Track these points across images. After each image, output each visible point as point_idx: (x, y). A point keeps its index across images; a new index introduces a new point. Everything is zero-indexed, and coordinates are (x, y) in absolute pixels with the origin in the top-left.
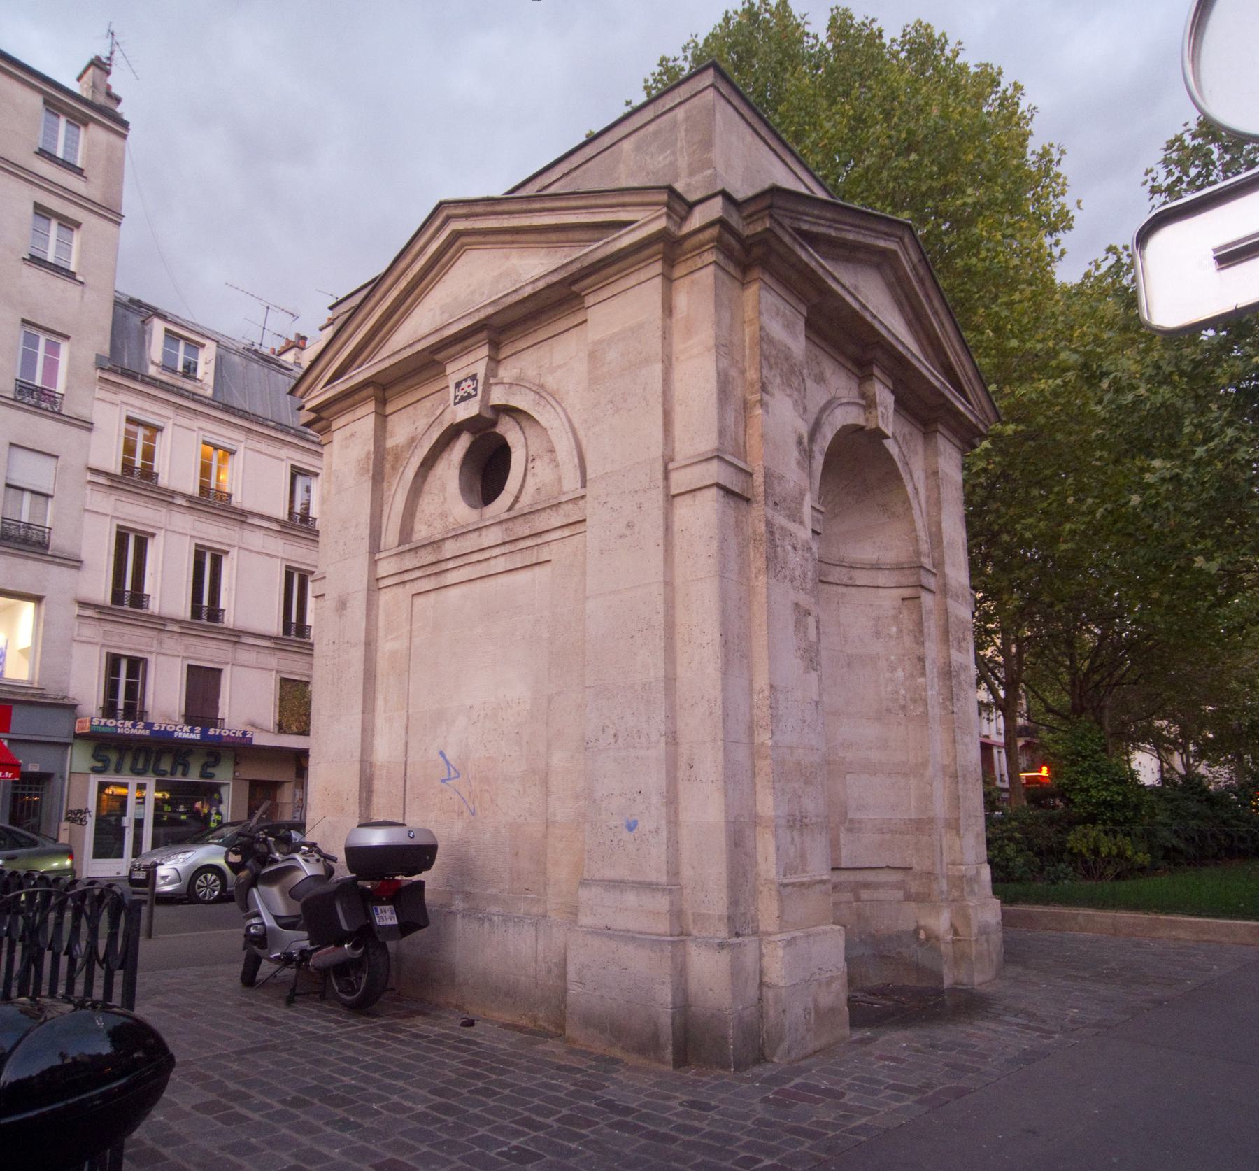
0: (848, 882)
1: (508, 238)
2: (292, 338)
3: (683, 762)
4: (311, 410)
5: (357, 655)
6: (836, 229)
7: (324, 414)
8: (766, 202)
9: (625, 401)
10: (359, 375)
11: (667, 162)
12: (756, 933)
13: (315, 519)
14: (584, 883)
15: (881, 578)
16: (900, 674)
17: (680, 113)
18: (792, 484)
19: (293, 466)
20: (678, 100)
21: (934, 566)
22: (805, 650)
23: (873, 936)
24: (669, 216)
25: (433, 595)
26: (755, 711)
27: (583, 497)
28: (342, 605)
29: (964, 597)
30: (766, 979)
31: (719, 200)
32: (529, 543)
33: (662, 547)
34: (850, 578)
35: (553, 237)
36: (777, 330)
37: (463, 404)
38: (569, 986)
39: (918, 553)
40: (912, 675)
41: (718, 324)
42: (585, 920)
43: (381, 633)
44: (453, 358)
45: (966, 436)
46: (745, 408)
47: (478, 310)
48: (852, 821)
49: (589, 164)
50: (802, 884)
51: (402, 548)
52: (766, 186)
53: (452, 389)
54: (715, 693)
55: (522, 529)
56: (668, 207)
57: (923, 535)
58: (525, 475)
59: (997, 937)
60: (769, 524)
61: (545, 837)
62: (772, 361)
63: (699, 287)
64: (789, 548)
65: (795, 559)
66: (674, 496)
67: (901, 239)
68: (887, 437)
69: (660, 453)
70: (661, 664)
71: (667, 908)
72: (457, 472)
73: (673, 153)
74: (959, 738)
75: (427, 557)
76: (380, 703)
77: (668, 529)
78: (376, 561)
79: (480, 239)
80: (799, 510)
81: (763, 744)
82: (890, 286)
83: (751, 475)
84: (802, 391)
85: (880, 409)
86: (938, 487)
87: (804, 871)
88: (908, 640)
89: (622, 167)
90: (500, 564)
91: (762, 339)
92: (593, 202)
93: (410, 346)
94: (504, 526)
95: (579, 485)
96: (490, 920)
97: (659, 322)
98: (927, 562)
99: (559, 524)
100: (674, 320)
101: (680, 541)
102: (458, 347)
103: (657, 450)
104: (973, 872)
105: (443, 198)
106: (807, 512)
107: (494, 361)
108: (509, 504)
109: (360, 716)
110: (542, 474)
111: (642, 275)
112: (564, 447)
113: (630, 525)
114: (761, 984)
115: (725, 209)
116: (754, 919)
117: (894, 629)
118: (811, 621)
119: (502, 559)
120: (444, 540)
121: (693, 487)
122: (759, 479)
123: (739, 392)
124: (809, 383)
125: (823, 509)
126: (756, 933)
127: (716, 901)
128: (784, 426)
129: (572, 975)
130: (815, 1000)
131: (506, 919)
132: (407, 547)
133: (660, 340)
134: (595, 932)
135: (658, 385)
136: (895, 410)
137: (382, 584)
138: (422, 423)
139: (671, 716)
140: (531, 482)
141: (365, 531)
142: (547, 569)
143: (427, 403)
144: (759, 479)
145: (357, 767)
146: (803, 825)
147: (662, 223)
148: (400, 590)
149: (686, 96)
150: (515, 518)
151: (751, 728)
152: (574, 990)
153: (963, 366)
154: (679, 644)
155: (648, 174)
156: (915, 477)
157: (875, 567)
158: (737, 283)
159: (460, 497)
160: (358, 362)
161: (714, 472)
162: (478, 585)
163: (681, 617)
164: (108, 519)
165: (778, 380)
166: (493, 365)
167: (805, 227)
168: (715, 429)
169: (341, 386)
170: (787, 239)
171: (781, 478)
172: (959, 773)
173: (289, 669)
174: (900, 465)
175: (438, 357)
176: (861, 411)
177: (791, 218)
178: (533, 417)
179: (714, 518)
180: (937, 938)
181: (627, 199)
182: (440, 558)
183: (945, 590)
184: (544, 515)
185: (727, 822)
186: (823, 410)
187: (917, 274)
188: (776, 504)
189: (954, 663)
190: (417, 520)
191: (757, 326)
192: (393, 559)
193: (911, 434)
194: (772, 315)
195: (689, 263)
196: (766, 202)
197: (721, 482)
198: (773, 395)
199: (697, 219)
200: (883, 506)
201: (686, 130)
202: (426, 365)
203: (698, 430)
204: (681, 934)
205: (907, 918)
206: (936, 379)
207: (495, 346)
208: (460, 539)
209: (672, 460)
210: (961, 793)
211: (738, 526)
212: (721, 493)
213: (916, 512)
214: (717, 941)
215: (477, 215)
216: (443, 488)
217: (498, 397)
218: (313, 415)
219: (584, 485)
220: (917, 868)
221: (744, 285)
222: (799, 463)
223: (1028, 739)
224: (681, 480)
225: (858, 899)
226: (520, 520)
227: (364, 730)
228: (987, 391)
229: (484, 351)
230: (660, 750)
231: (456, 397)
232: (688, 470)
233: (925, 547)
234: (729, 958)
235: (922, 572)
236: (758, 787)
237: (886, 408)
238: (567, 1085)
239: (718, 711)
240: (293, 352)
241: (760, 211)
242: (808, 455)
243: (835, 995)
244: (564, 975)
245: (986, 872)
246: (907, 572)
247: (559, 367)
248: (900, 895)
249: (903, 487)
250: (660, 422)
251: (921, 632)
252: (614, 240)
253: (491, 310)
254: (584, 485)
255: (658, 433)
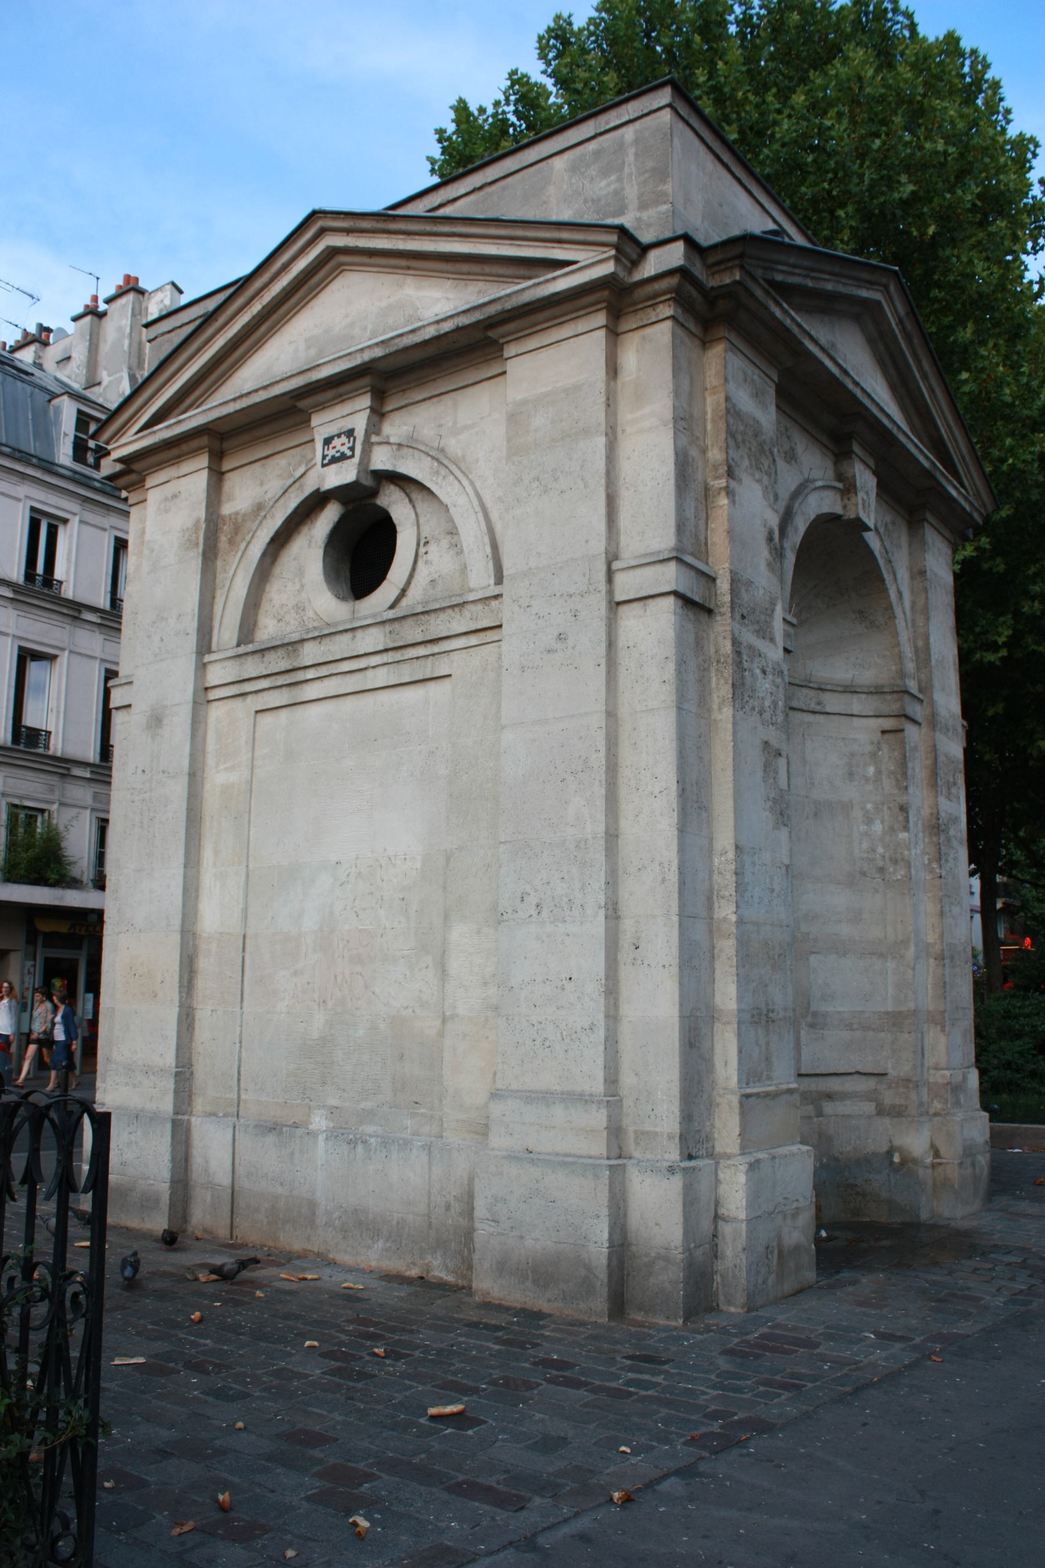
0: (815, 1091)
1: (403, 263)
2: (32, 329)
3: (626, 941)
4: (120, 460)
5: (178, 789)
6: (812, 278)
7: (136, 466)
8: (738, 250)
9: (556, 480)
10: (193, 419)
11: (613, 187)
12: (711, 1155)
13: (61, 583)
14: (495, 1095)
15: (857, 704)
16: (878, 827)
17: (629, 133)
18: (761, 592)
19: (33, 509)
20: (626, 118)
21: (920, 691)
22: (775, 801)
23: (837, 1159)
24: (617, 259)
25: (284, 714)
26: (715, 877)
27: (497, 597)
28: (156, 721)
29: (955, 730)
30: (722, 1211)
31: (679, 247)
32: (421, 651)
33: (603, 667)
34: (819, 704)
35: (465, 267)
36: (745, 401)
37: (334, 467)
38: (477, 1225)
39: (902, 674)
40: (892, 829)
41: (676, 393)
42: (498, 1140)
43: (210, 760)
44: (322, 407)
45: (958, 527)
46: (706, 496)
47: (362, 350)
48: (815, 1014)
49: (510, 179)
50: (767, 1095)
51: (242, 649)
52: (736, 232)
53: (319, 445)
54: (670, 855)
55: (412, 632)
56: (618, 249)
57: (908, 651)
58: (415, 562)
59: (983, 1160)
60: (735, 642)
61: (441, 1034)
62: (740, 438)
63: (652, 347)
64: (758, 671)
65: (764, 686)
66: (618, 604)
67: (886, 287)
68: (867, 529)
69: (603, 549)
70: (601, 816)
71: (605, 1124)
72: (320, 553)
73: (620, 180)
74: (946, 909)
75: (277, 662)
76: (208, 855)
77: (611, 644)
78: (205, 665)
79: (365, 260)
80: (769, 624)
81: (725, 919)
82: (870, 341)
83: (714, 580)
84: (772, 473)
85: (861, 495)
86: (926, 590)
87: (769, 1078)
88: (888, 784)
89: (551, 190)
90: (381, 677)
91: (728, 411)
92: (520, 233)
93: (265, 388)
94: (388, 628)
95: (492, 581)
96: (364, 1142)
97: (601, 386)
98: (913, 686)
99: (464, 630)
100: (619, 382)
101: (626, 661)
102: (330, 394)
103: (598, 545)
104: (960, 1078)
105: (317, 207)
106: (778, 627)
107: (378, 414)
108: (392, 598)
109: (181, 871)
110: (439, 561)
111: (581, 326)
112: (471, 531)
113: (561, 637)
114: (717, 1217)
115: (687, 256)
116: (709, 1138)
117: (871, 770)
118: (782, 762)
119: (383, 671)
120: (302, 641)
121: (644, 594)
122: (724, 585)
123: (699, 476)
124: (781, 464)
125: (794, 621)
126: (711, 1155)
127: (664, 1116)
128: (748, 518)
129: (480, 1210)
130: (779, 1237)
131: (386, 1143)
132: (250, 648)
133: (603, 407)
134: (513, 1157)
135: (600, 464)
136: (877, 494)
137: (213, 695)
138: (274, 486)
139: (612, 882)
140: (422, 571)
141: (192, 625)
142: (445, 685)
143: (282, 461)
144: (724, 585)
145: (177, 938)
146: (770, 1021)
147: (609, 268)
148: (238, 703)
149: (636, 115)
150: (404, 617)
151: (710, 900)
152: (483, 1230)
153: (956, 441)
154: (623, 791)
155: (585, 201)
156: (899, 576)
157: (850, 690)
158: (697, 342)
159: (324, 586)
160: (188, 402)
161: (669, 576)
162: (349, 703)
163: (626, 756)
164: (96, 664)
165: (746, 463)
166: (376, 419)
167: (779, 277)
168: (672, 521)
169: (163, 432)
170: (759, 293)
171: (749, 583)
172: (947, 954)
173: (21, 792)
174: (881, 562)
175: (302, 404)
176: (838, 497)
177: (765, 268)
178: (428, 490)
179: (670, 634)
180: (914, 1161)
181: (565, 235)
182: (296, 665)
183: (933, 722)
184: (443, 616)
185: (682, 1017)
186: (796, 495)
187: (903, 329)
188: (743, 617)
189: (943, 815)
190: (262, 611)
191: (722, 395)
192: (229, 664)
193: (894, 523)
194: (729, 376)
195: (640, 315)
196: (738, 250)
197: (681, 590)
198: (740, 481)
199: (654, 264)
200: (861, 612)
201: (636, 154)
202: (283, 415)
203: (651, 520)
204: (620, 1157)
205: (880, 1136)
206: (925, 457)
207: (380, 396)
208: (326, 641)
209: (616, 557)
210: (947, 979)
211: (699, 644)
212: (680, 602)
213: (900, 622)
214: (666, 1164)
215: (362, 231)
216: (301, 572)
217: (382, 460)
218: (119, 467)
219: (499, 580)
220: (893, 1073)
221: (705, 344)
222: (769, 565)
223: (1010, 901)
224: (627, 585)
225: (820, 1114)
226: (410, 622)
227: (186, 890)
228: (983, 472)
229: (365, 401)
230: (598, 926)
231: (324, 457)
232: (638, 572)
233: (910, 666)
234: (680, 1184)
235: (907, 698)
236: (718, 974)
237: (867, 493)
238: (547, 1333)
239: (673, 877)
240: (31, 350)
241: (729, 260)
242: (778, 553)
243: (798, 1233)
244: (469, 1212)
245: (973, 1078)
246: (889, 697)
247: (466, 428)
248: (869, 1108)
249: (885, 590)
250: (602, 510)
251: (905, 774)
252: (547, 281)
253: (378, 352)
254: (499, 580)
255: (601, 526)
